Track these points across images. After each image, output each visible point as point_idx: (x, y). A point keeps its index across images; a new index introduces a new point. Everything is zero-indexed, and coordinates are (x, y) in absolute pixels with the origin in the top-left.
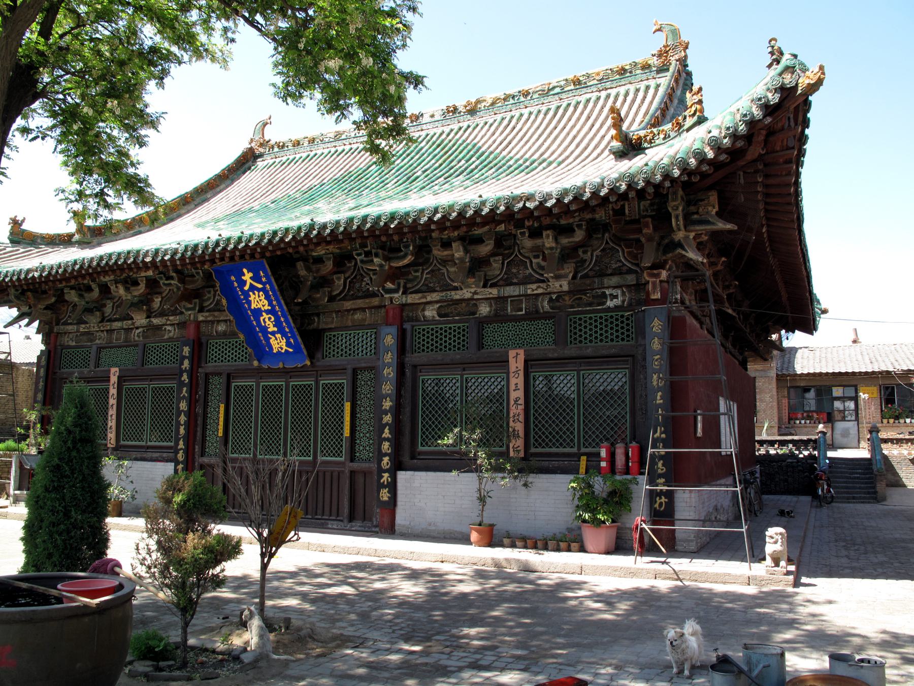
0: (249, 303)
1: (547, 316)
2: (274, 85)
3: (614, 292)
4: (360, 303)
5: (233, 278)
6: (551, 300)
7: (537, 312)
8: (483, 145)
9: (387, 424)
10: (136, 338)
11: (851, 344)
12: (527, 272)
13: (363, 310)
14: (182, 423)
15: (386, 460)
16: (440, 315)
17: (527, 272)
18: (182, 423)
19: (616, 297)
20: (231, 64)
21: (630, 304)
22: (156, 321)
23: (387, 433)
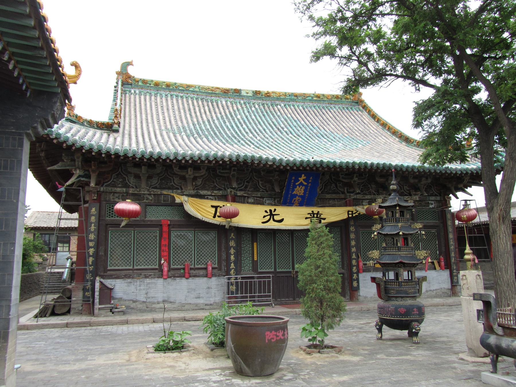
0: (293, 191)
2: (410, 84)
4: (334, 196)
8: (145, 100)
9: (354, 252)
12: (171, 184)
13: (334, 199)
14: (232, 253)
17: (171, 184)
18: (232, 253)
19: (432, 204)
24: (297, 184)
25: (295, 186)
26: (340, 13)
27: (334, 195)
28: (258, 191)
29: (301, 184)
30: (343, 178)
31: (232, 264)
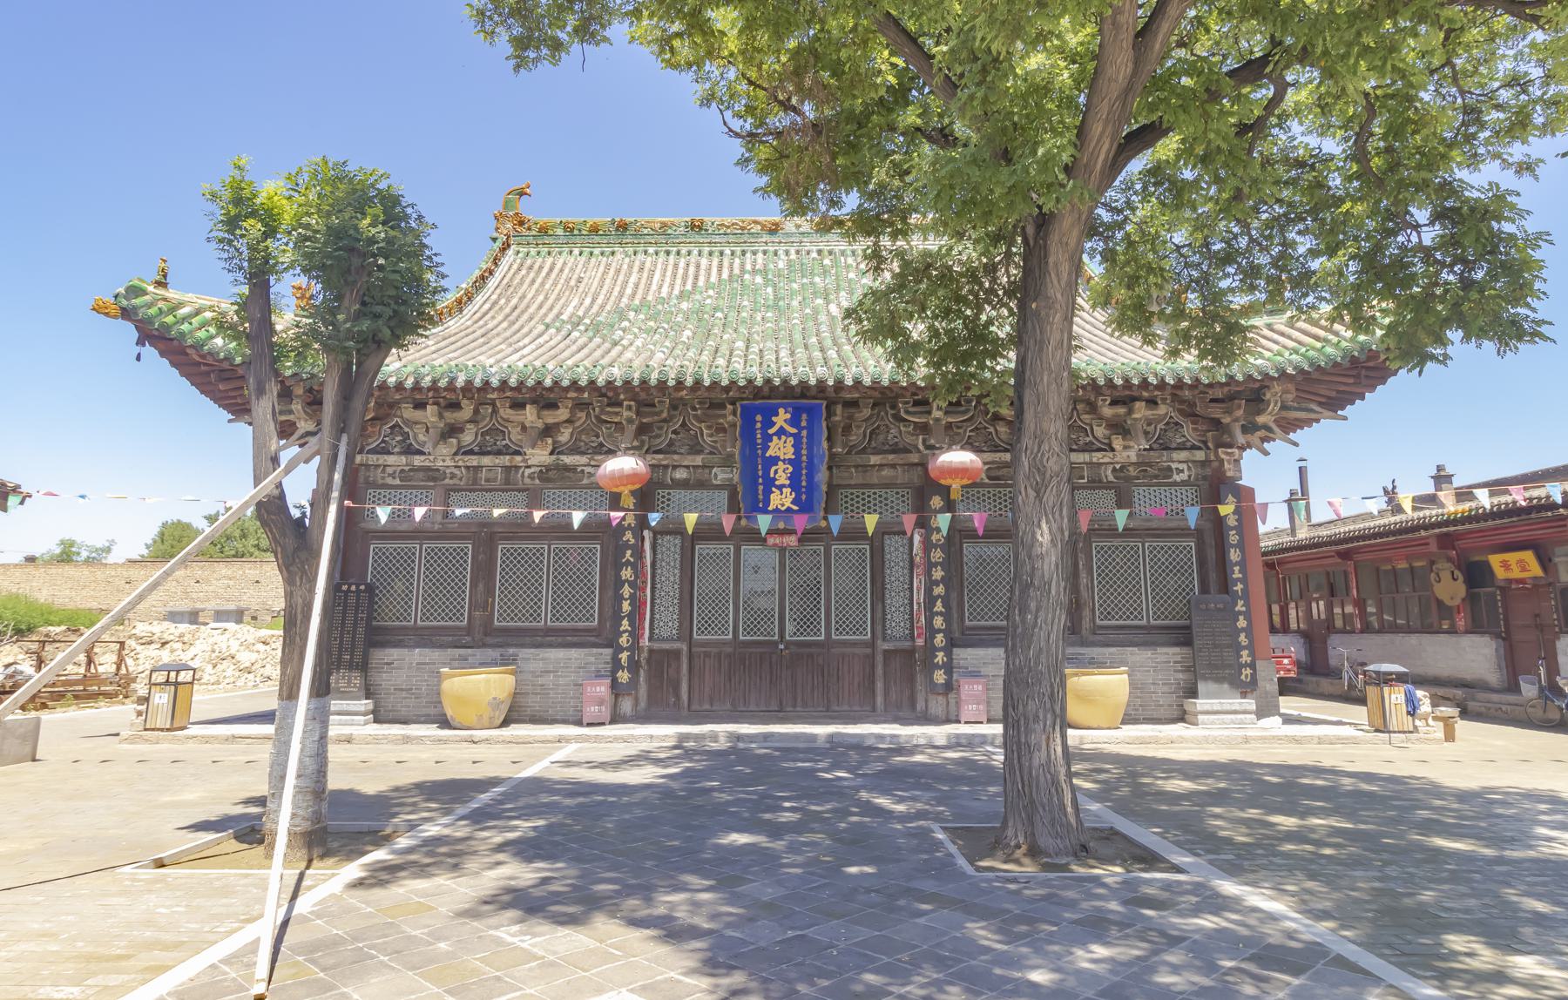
0: (766, 448)
1: (1108, 486)
3: (1181, 466)
5: (759, 418)
6: (1114, 470)
7: (1100, 481)
9: (939, 596)
10: (527, 481)
11: (35, 495)
13: (893, 466)
15: (940, 637)
16: (989, 478)
20: (738, 168)
21: (1197, 479)
22: (568, 460)
23: (939, 607)
24: (771, 431)
25: (768, 438)
26: (676, 43)
27: (891, 457)
28: (699, 452)
29: (781, 432)
30: (907, 412)
31: (625, 622)
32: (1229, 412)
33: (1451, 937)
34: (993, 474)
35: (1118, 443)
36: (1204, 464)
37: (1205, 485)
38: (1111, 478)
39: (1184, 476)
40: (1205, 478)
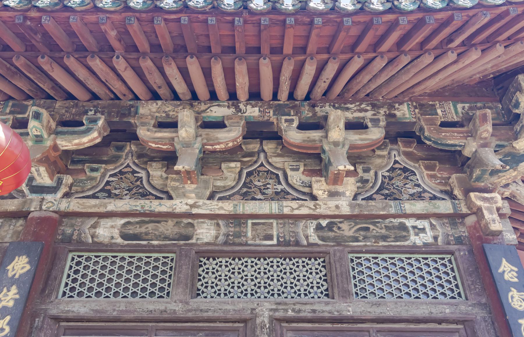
6: (319, 228)
7: (297, 243)
16: (124, 236)
32: (472, 134)
33: (321, 8)
34: (131, 230)
35: (320, 187)
36: (455, 218)
37: (462, 252)
38: (314, 238)
39: (427, 237)
40: (459, 241)
